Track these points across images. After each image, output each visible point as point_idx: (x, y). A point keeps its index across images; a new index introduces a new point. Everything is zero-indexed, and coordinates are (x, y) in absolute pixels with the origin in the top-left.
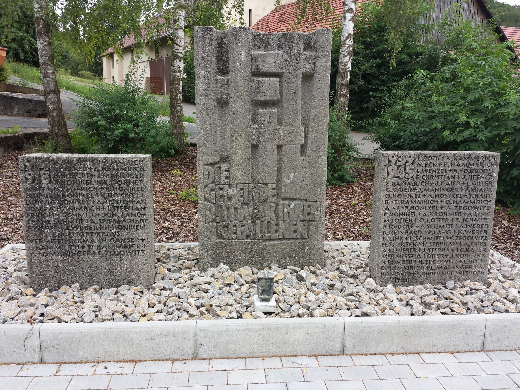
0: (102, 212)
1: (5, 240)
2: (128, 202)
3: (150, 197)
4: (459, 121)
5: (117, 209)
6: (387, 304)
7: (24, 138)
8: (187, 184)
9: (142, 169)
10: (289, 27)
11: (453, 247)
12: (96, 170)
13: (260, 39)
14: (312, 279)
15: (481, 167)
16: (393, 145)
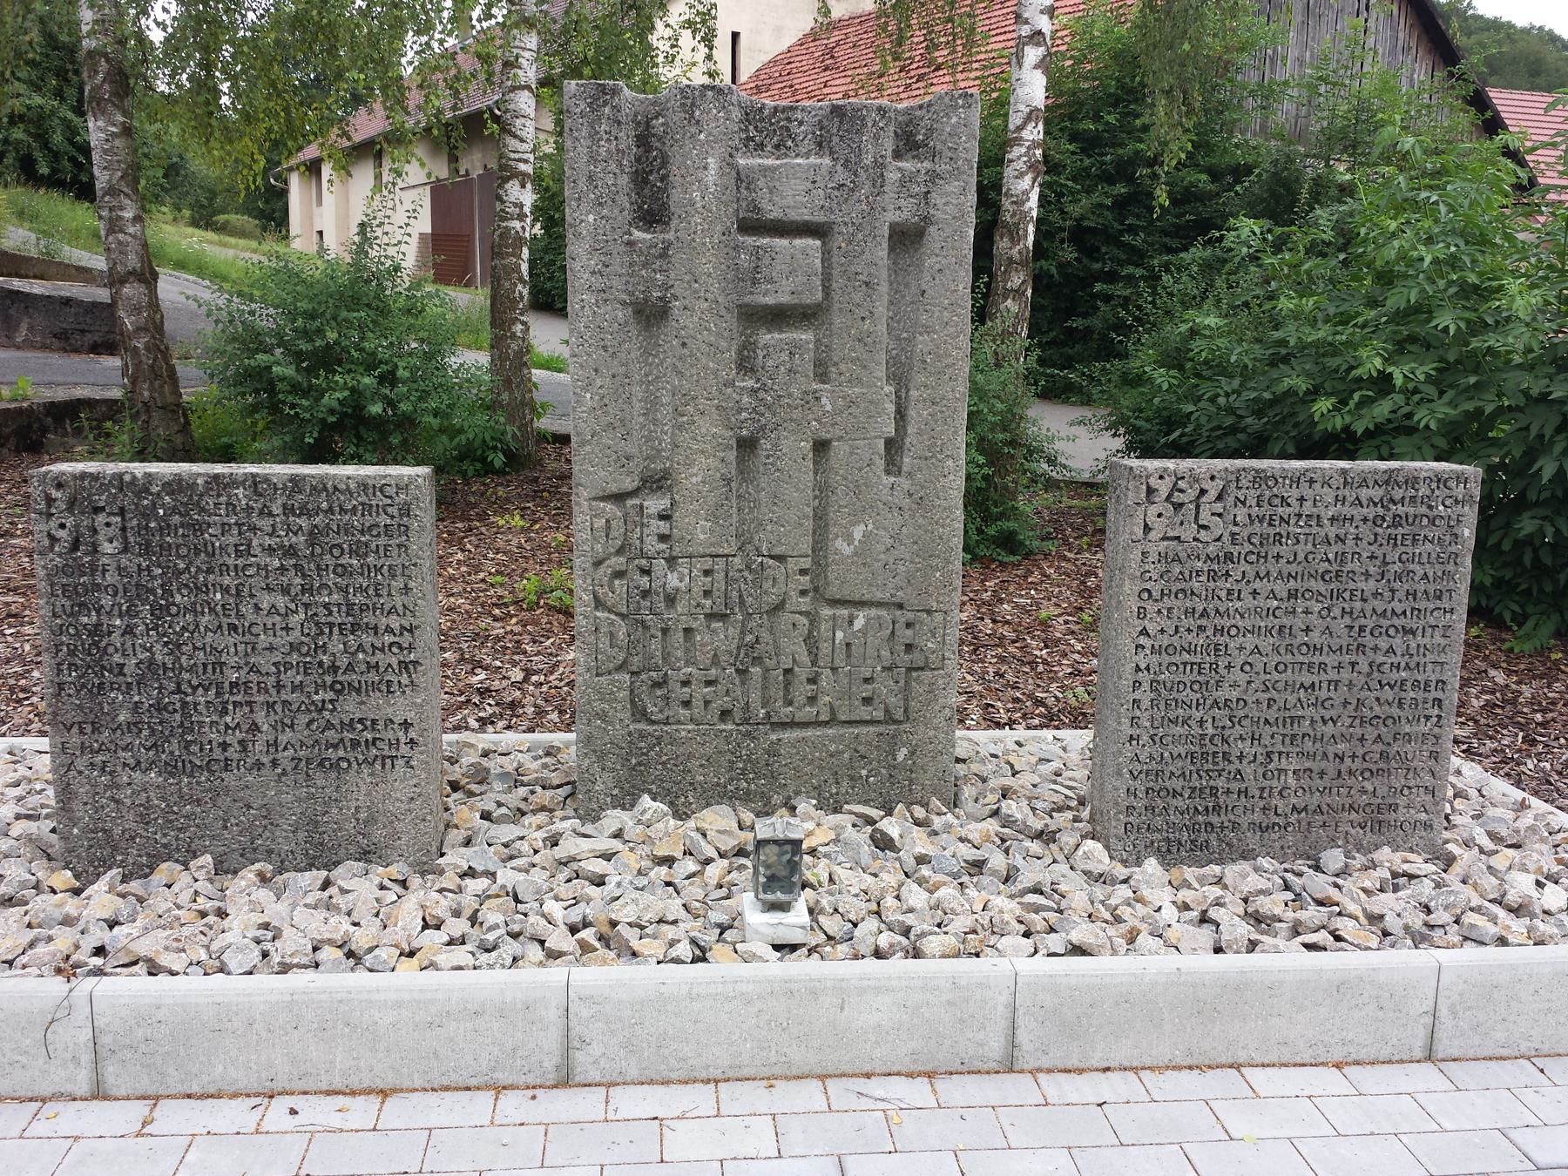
0: (282, 640)
2: (362, 610)
3: (428, 597)
5: (327, 631)
6: (1143, 920)
7: (48, 414)
8: (542, 556)
9: (406, 510)
10: (853, 86)
12: (265, 512)
14: (919, 842)
16: (1163, 441)
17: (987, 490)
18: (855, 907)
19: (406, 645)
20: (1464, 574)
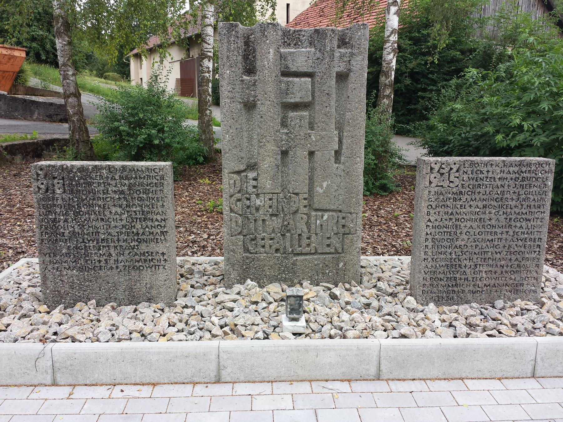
0: (119, 224)
1: (20, 253)
2: (147, 213)
3: (170, 208)
4: (511, 124)
5: (135, 220)
6: (428, 325)
7: (44, 144)
8: (215, 194)
9: (162, 178)
10: (330, 22)
11: (503, 263)
12: (113, 178)
13: (290, 35)
14: (347, 297)
15: (534, 175)
16: (441, 150)
17: (376, 169)
18: (323, 320)
19: (163, 226)
20: (549, 199)
